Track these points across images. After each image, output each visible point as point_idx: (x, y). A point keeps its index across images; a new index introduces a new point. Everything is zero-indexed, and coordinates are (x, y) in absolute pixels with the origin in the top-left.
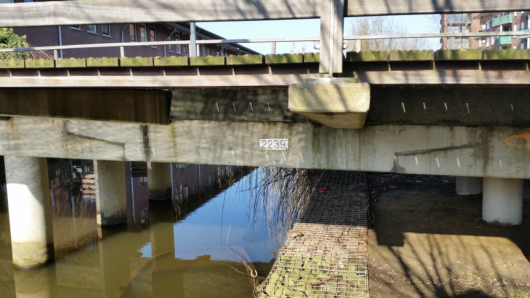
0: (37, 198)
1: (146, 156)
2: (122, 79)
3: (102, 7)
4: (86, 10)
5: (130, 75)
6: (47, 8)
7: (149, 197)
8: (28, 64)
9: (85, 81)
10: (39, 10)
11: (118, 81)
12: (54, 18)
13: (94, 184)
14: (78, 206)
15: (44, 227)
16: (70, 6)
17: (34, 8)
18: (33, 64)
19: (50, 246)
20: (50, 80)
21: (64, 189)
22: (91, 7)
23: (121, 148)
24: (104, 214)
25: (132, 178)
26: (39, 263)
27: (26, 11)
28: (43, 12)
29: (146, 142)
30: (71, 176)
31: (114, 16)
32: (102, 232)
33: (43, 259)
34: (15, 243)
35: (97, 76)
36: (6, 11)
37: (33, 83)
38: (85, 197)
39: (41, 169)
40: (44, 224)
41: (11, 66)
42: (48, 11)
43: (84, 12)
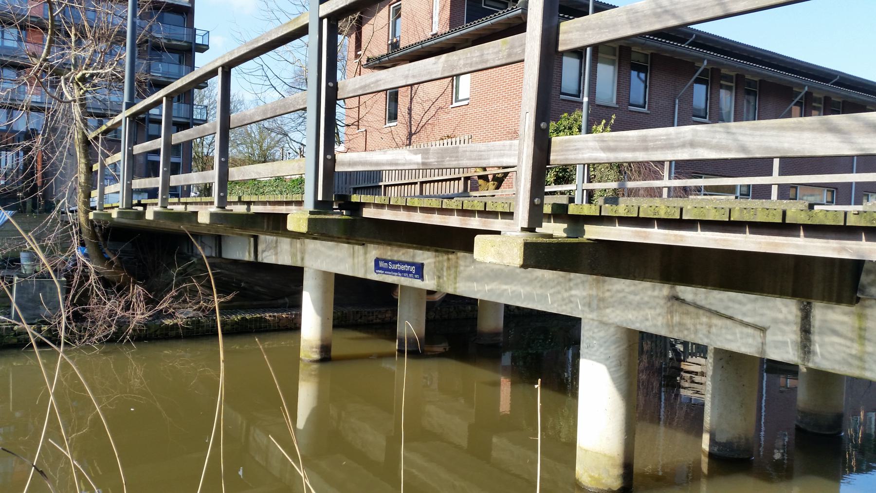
0: (619, 390)
1: (802, 355)
2: (785, 242)
3: (767, 133)
4: (740, 138)
5: (799, 236)
6: (682, 135)
7: (795, 422)
8: (644, 212)
9: (724, 240)
10: (669, 139)
11: (777, 245)
12: (690, 149)
13: (703, 374)
14: (671, 407)
15: (623, 436)
16: (715, 132)
17: (663, 136)
18: (649, 212)
19: (628, 467)
20: (671, 235)
21: (654, 373)
22: (748, 132)
23: (757, 333)
24: (715, 435)
25: (765, 374)
26: (610, 489)
27: (651, 141)
28: (675, 142)
29: (806, 330)
30: (666, 355)
31: (786, 145)
32: (709, 464)
33: (615, 483)
34: (581, 449)
35: (745, 235)
36: (626, 141)
37: (645, 237)
38: (683, 392)
39: (630, 346)
40: (624, 431)
41: (620, 213)
42: (682, 140)
43: (736, 140)
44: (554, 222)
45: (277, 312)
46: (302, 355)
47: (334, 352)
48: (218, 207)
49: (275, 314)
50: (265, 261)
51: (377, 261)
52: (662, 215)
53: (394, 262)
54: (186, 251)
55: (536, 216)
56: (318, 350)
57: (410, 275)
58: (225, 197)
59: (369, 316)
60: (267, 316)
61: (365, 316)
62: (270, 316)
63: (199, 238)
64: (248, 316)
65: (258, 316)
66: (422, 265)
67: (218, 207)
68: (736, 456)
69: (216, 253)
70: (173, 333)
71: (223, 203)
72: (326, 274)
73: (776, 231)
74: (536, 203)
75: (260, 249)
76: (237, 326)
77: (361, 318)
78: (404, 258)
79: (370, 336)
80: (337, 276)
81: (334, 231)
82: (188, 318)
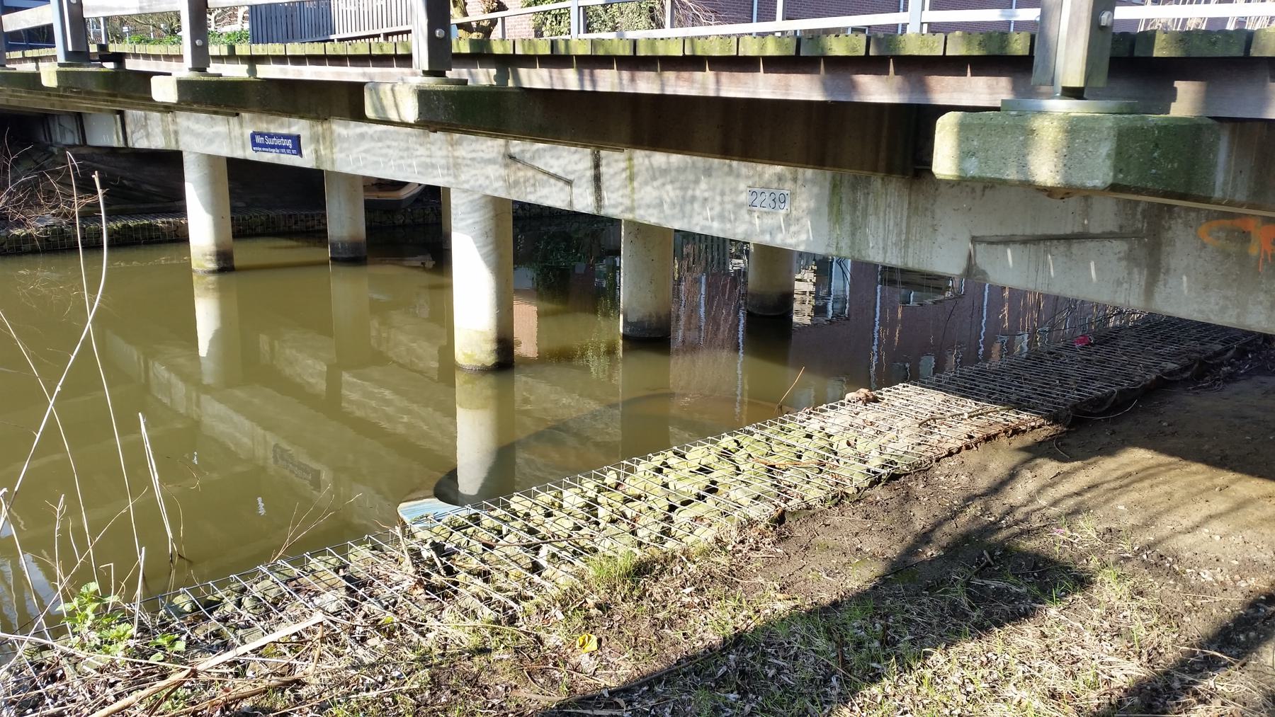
26: (483, 365)
37: (286, 73)
39: (497, 215)
44: (765, 72)
45: (173, 217)
46: (194, 266)
47: (237, 262)
48: (193, 69)
49: (171, 220)
50: (137, 146)
51: (253, 136)
52: (716, 52)
53: (270, 136)
54: (43, 138)
55: (441, 56)
56: (213, 258)
57: (288, 151)
58: (205, 47)
59: (308, 221)
60: (159, 222)
61: (302, 221)
62: (163, 223)
63: (56, 118)
64: (131, 223)
65: (146, 222)
66: (298, 137)
67: (193, 69)
68: (647, 335)
69: (79, 139)
70: (29, 247)
71: (201, 58)
72: (212, 160)
73: (337, 63)
74: (437, 35)
75: (128, 130)
76: (117, 236)
77: (296, 223)
78: (284, 131)
79: (300, 244)
80: (209, 156)
81: (93, 86)
82: (46, 226)
